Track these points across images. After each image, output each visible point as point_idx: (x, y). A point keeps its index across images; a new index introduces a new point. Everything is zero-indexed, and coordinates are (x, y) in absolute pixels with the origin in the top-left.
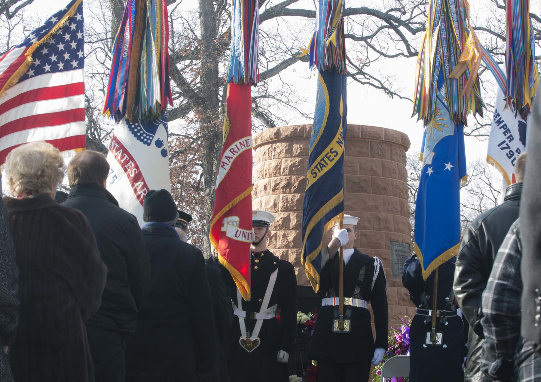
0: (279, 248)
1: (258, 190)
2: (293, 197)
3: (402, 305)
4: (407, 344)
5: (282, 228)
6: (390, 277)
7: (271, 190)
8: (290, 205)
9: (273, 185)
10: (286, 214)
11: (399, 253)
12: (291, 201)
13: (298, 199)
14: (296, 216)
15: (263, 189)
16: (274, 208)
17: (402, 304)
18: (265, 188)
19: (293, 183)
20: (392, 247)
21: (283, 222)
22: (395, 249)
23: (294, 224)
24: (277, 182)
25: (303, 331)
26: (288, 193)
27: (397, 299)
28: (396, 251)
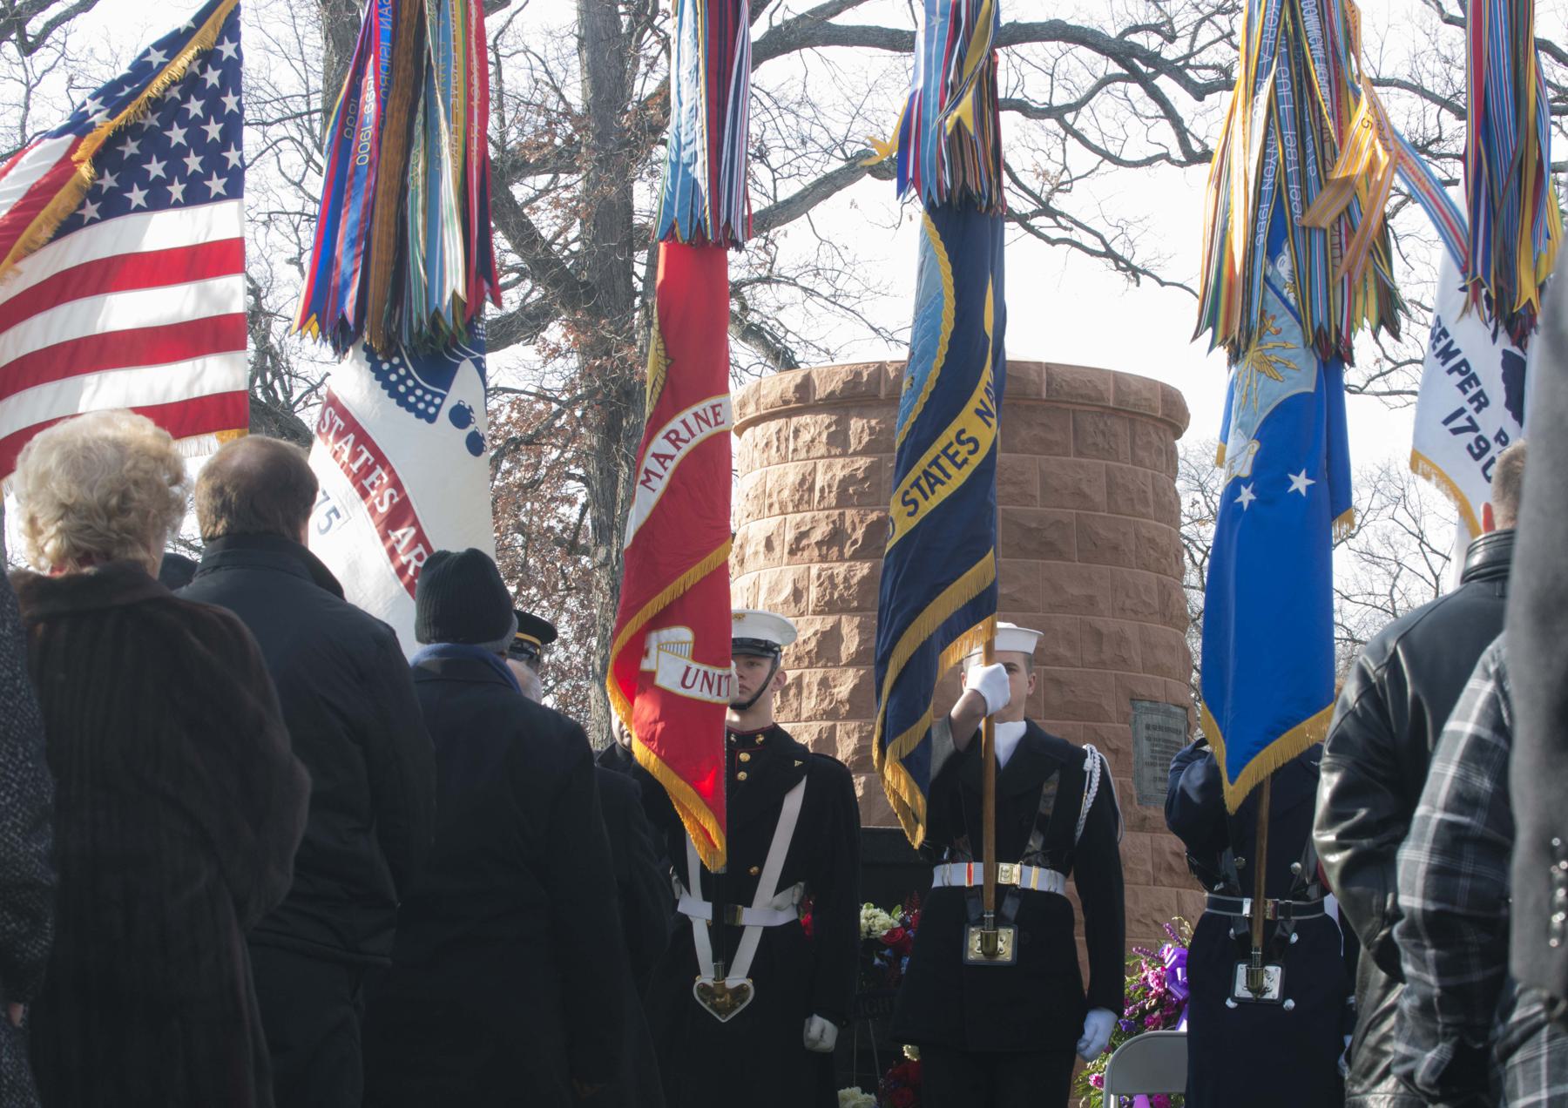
0: (809, 719)
1: (749, 551)
2: (850, 571)
3: (1164, 886)
4: (1181, 997)
6: (1131, 803)
7: (786, 550)
8: (841, 596)
9: (790, 536)
10: (830, 621)
11: (1157, 734)
12: (844, 582)
14: (858, 627)
15: (762, 548)
16: (793, 604)
17: (1165, 883)
18: (769, 545)
19: (849, 531)
20: (1135, 716)
21: (819, 643)
22: (1145, 722)
23: (853, 649)
24: (803, 529)
25: (877, 961)
26: (834, 559)
27: (1149, 868)
28: (1148, 727)
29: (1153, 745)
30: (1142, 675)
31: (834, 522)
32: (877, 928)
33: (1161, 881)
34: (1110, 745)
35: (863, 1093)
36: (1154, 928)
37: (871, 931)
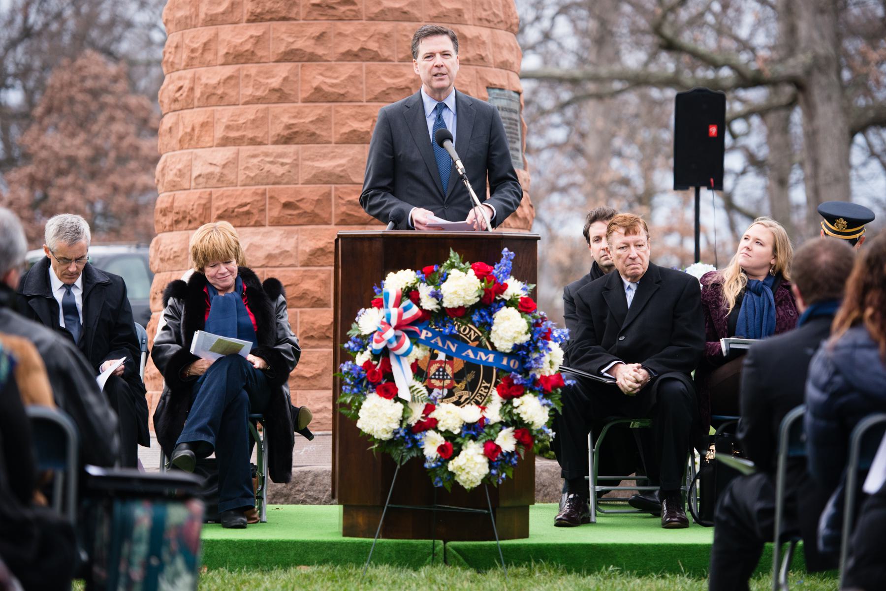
3: (511, 228)
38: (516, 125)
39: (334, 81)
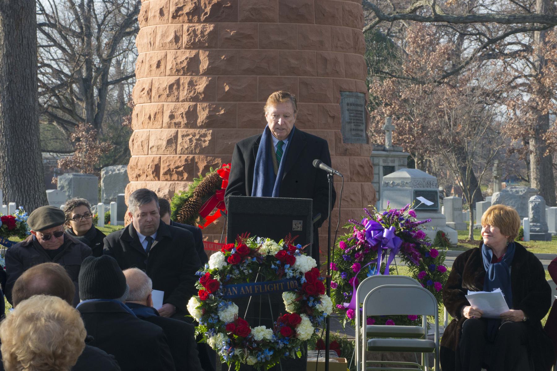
0: (183, 101)
1: (150, 15)
2: (204, 28)
3: (355, 182)
4: (373, 245)
5: (187, 73)
6: (340, 142)
7: (171, 16)
8: (199, 40)
9: (173, 9)
10: (194, 52)
11: (352, 108)
12: (201, 34)
13: (210, 31)
14: (208, 56)
15: (158, 14)
16: (174, 44)
17: (356, 180)
18: (162, 13)
19: (203, 8)
20: (342, 99)
21: (188, 63)
22: (346, 102)
23: (205, 67)
24: (179, 6)
25: (273, 266)
26: (196, 22)
27: (349, 173)
28: (348, 104)
29: (350, 113)
30: (345, 79)
31: (195, 3)
32: (272, 250)
33: (354, 180)
34: (330, 113)
35: (267, 328)
36: (351, 203)
37: (269, 251)
38: (361, 114)
39: (239, 88)
